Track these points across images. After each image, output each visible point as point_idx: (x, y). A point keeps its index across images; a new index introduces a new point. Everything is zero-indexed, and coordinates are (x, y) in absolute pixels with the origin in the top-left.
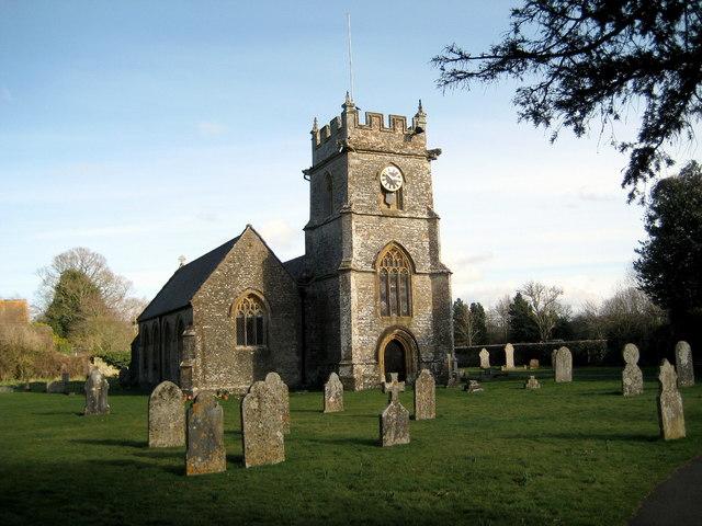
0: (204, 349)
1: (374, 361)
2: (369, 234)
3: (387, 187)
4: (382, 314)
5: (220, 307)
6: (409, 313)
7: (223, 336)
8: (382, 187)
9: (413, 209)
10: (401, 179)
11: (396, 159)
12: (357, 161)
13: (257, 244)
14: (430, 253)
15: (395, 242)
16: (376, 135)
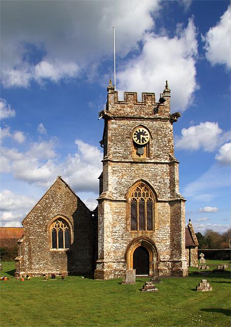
0: (30, 250)
1: (123, 260)
2: (123, 175)
3: (138, 142)
4: (132, 229)
5: (40, 226)
6: (151, 228)
7: (42, 243)
8: (135, 144)
9: (158, 156)
10: (149, 136)
11: (145, 123)
12: (115, 126)
13: (63, 186)
14: (170, 187)
15: (142, 180)
16: (131, 107)
